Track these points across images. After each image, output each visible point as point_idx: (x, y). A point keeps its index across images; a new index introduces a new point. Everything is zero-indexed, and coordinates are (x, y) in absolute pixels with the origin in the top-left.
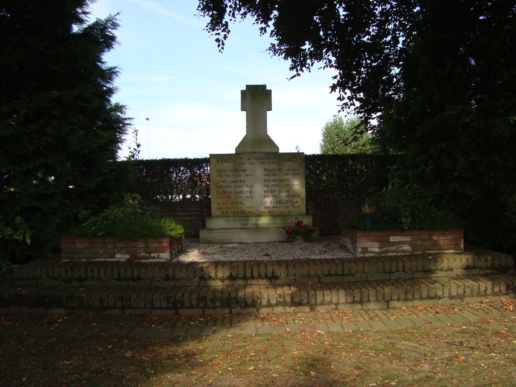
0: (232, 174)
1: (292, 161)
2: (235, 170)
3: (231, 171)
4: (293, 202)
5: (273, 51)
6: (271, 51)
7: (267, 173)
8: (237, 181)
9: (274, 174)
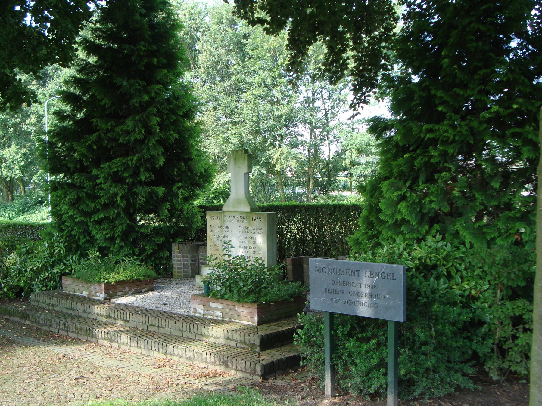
0: (219, 229)
2: (222, 227)
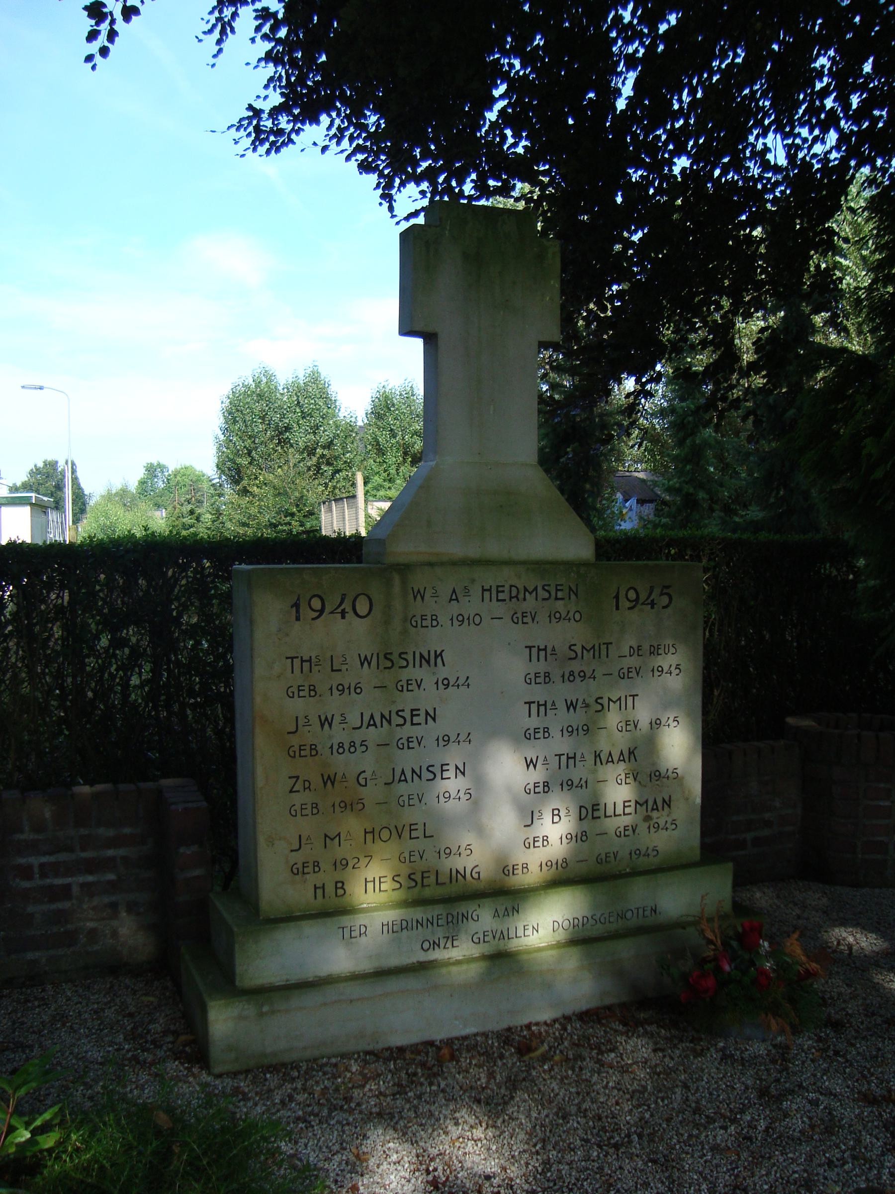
0: (367, 676)
1: (653, 604)
3: (365, 661)
4: (650, 803)
5: (249, 135)
6: (242, 133)
7: (541, 667)
8: (394, 715)
9: (572, 673)
